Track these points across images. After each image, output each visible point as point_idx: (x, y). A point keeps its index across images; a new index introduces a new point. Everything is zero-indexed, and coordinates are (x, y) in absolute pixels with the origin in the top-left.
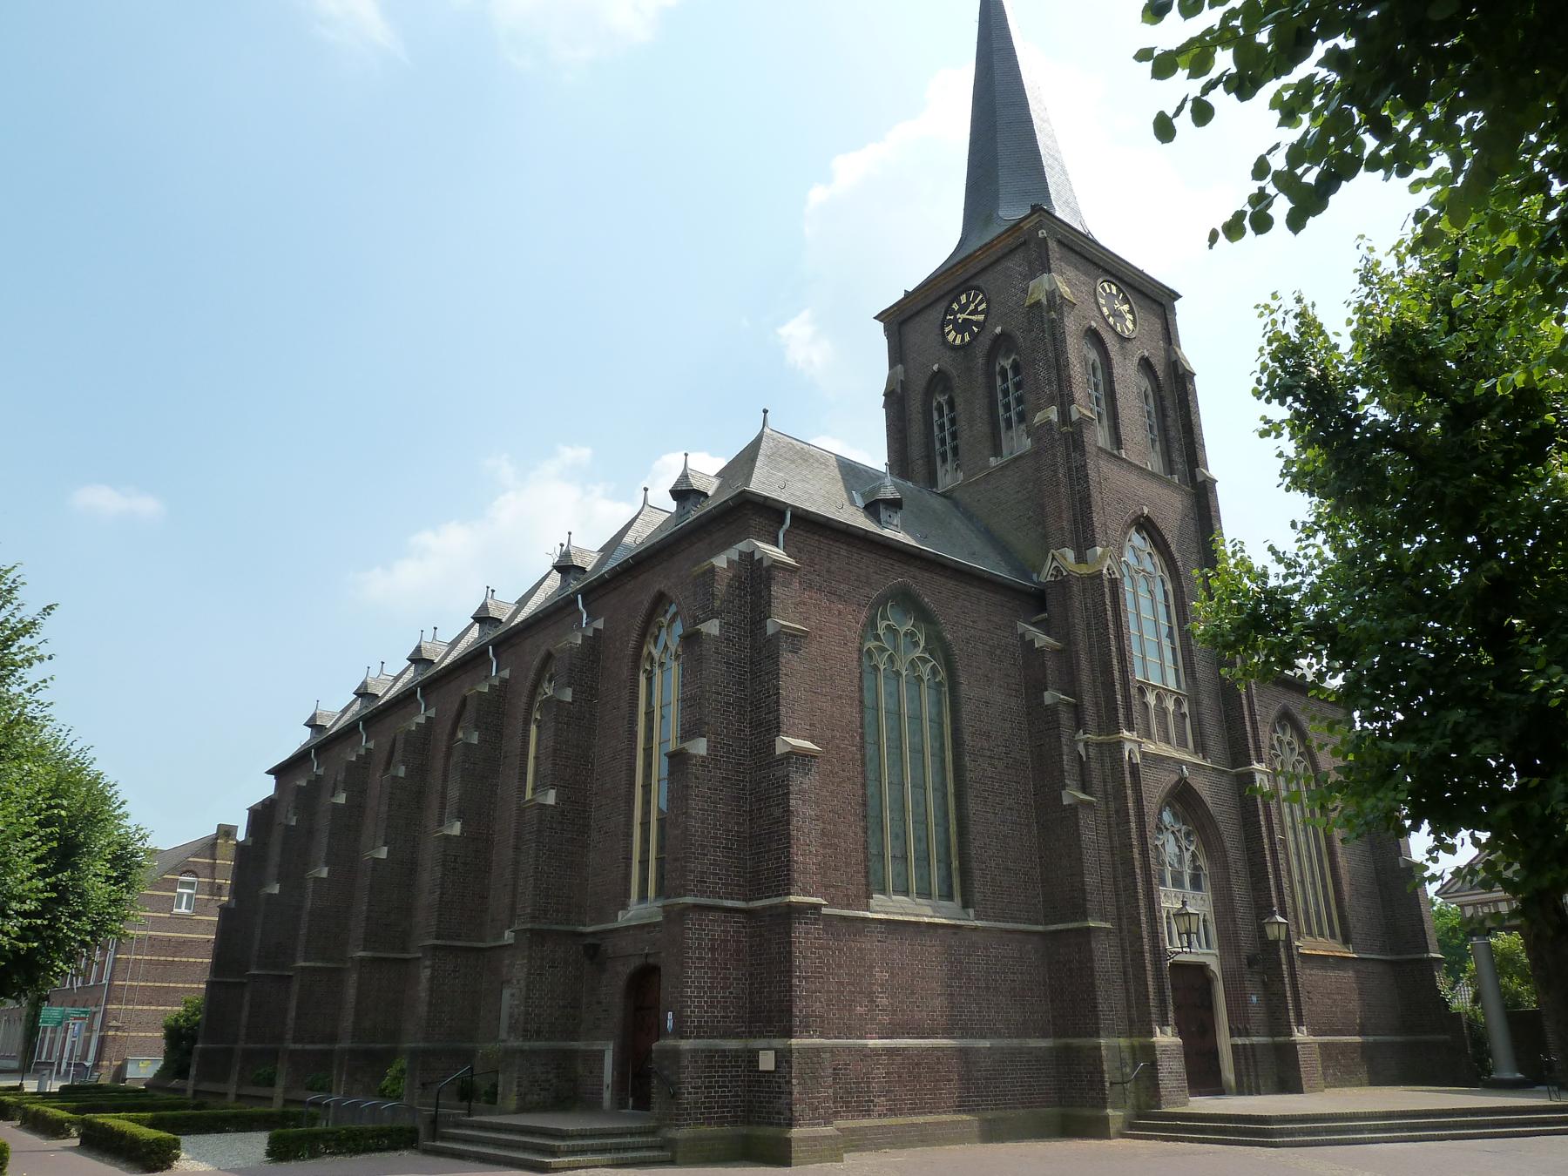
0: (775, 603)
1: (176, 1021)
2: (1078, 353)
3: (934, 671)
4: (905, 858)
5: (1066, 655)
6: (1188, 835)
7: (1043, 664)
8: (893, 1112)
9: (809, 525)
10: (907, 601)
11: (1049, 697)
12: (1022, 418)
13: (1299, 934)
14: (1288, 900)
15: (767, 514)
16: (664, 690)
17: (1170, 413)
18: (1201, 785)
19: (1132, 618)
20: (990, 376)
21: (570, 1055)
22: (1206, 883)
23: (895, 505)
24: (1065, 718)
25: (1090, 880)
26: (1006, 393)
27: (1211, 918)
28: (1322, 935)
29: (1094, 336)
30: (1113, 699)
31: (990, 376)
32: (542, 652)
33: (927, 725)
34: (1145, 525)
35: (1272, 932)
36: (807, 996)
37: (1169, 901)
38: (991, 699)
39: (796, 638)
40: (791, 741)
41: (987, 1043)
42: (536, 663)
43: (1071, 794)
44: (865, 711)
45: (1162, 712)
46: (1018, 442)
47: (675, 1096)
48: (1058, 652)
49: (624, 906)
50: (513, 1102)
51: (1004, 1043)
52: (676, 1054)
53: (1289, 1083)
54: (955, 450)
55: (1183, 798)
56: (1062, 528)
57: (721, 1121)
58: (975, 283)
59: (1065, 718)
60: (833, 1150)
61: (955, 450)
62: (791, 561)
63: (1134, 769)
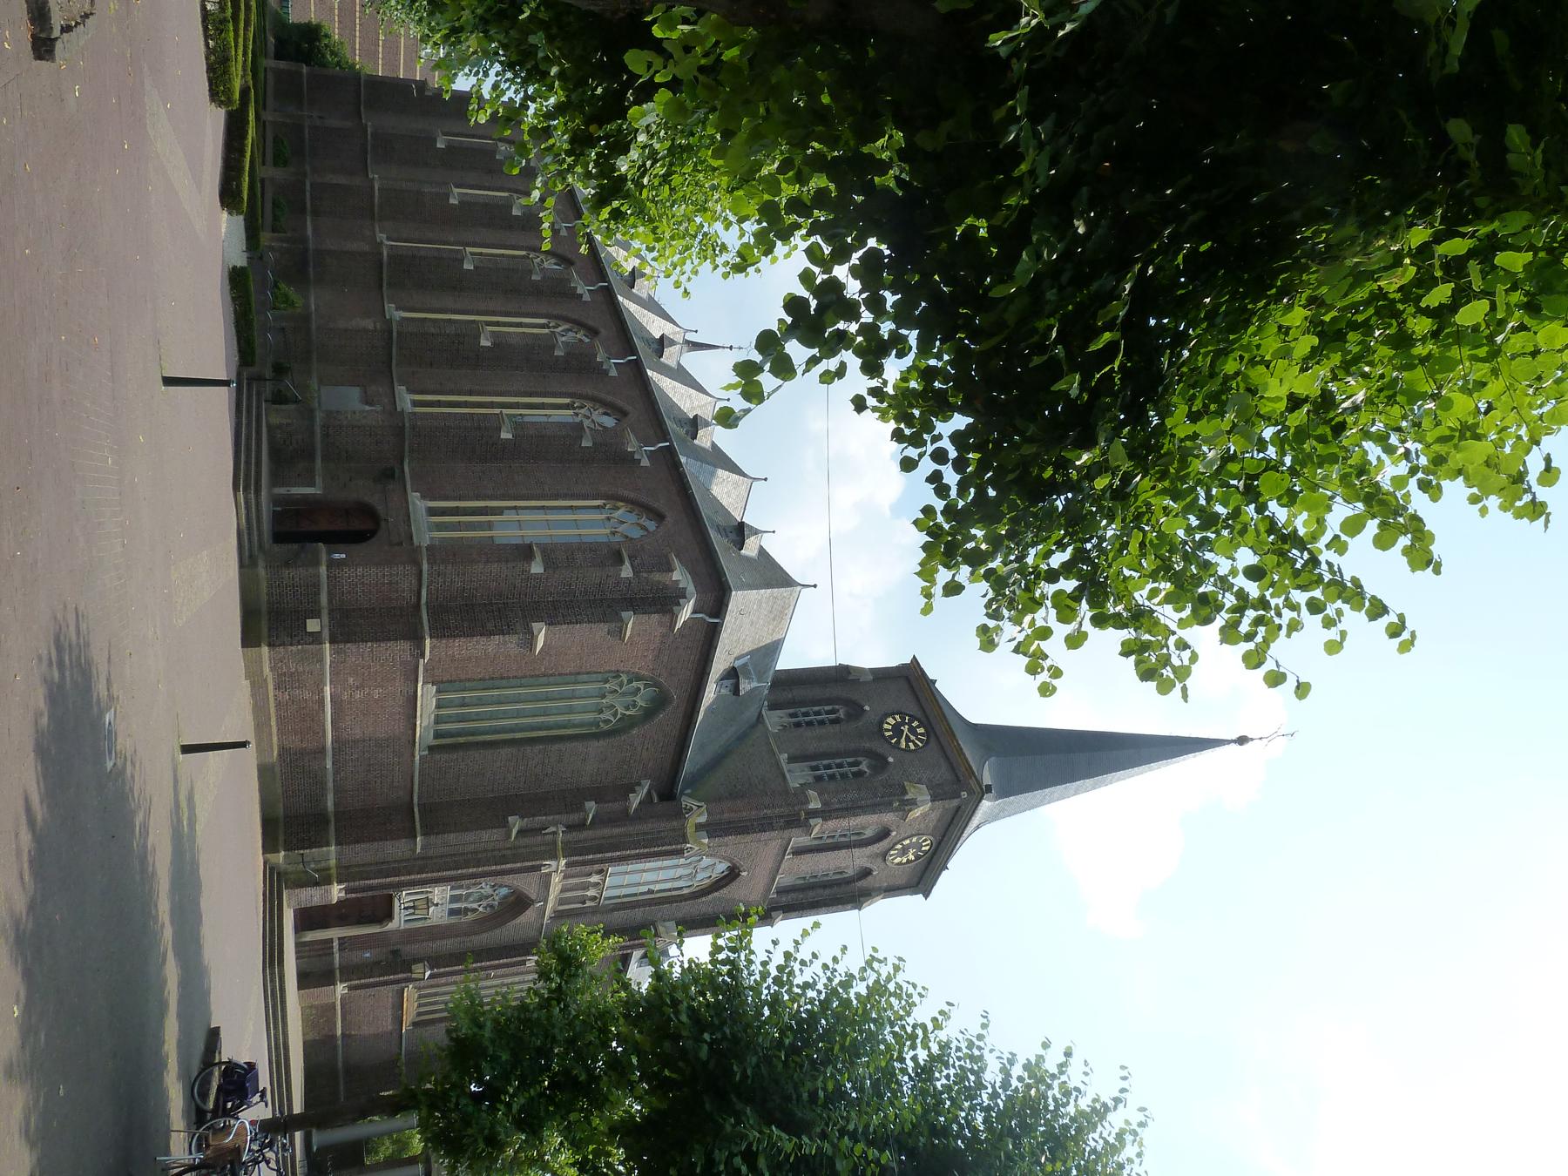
0: (646, 617)
1: (326, 36)
2: (869, 823)
3: (607, 721)
4: (463, 705)
5: (623, 817)
6: (492, 906)
7: (615, 800)
8: (278, 705)
9: (711, 636)
10: (660, 702)
11: (591, 806)
12: (819, 779)
13: (419, 989)
14: (443, 980)
15: (716, 601)
17: (827, 892)
18: (528, 916)
19: (659, 864)
20: (855, 753)
21: (311, 457)
22: (454, 919)
23: (736, 690)
24: (574, 818)
26: (840, 766)
27: (428, 923)
28: (420, 1006)
29: (884, 834)
30: (593, 850)
31: (855, 753)
32: (628, 408)
33: (566, 717)
34: (732, 874)
35: (418, 969)
36: (358, 653)
37: (440, 893)
38: (589, 762)
39: (620, 633)
41: (329, 765)
42: (619, 403)
43: (516, 823)
44: (574, 677)
45: (586, 887)
46: (797, 776)
47: (287, 564)
48: (626, 809)
49: (423, 497)
50: (275, 420)
51: (330, 778)
52: (317, 564)
53: (305, 980)
54: (798, 725)
55: (518, 903)
56: (723, 812)
57: (270, 594)
58: (933, 739)
59: (574, 818)
60: (254, 676)
61: (798, 725)
62: (679, 625)
63: (538, 868)
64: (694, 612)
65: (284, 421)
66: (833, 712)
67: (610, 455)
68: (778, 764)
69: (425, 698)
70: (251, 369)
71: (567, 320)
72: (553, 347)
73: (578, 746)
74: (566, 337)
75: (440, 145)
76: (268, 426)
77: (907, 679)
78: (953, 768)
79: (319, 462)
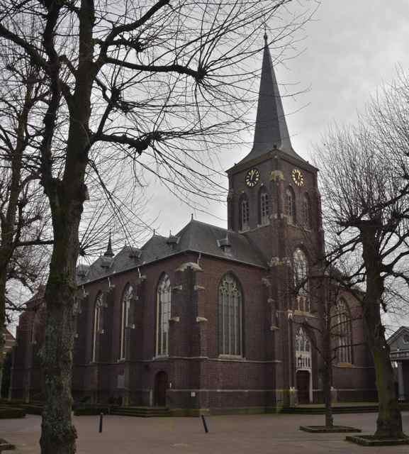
3: (238, 294)
10: (232, 275)
16: (165, 298)
25: (276, 350)
40: (199, 319)
42: (125, 284)
43: (273, 327)
46: (266, 222)
49: (155, 356)
58: (257, 167)
59: (273, 307)
61: (248, 219)
64: (197, 263)
66: (244, 205)
67: (142, 289)
68: (261, 228)
71: (96, 301)
72: (104, 308)
74: (101, 302)
75: (35, 342)
77: (233, 175)
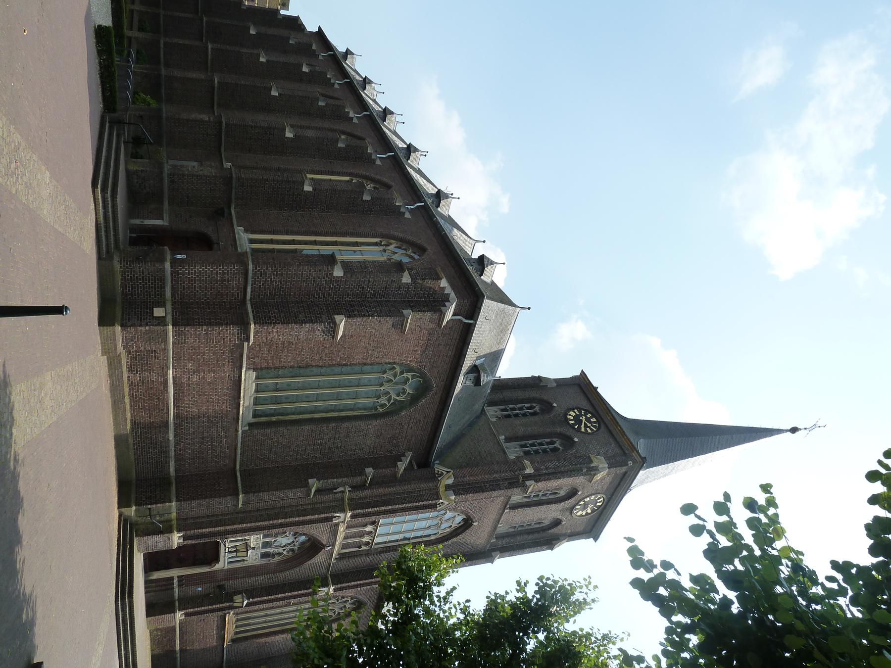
0: (421, 314)
2: (564, 484)
3: (383, 405)
4: (277, 390)
5: (393, 480)
6: (293, 550)
7: (388, 467)
8: (131, 384)
9: (465, 333)
10: (423, 390)
11: (369, 471)
12: (527, 453)
13: (237, 614)
14: (256, 607)
16: (371, 252)
17: (531, 537)
18: (321, 557)
22: (265, 561)
23: (477, 382)
24: (358, 480)
25: (266, 495)
26: (541, 444)
27: (245, 564)
28: (237, 627)
29: (573, 493)
30: (369, 507)
33: (352, 402)
34: (467, 524)
35: (238, 599)
36: (197, 335)
37: (255, 540)
38: (367, 438)
40: (342, 324)
41: (171, 438)
42: (385, 180)
44: (359, 366)
45: (362, 535)
46: (513, 452)
47: (138, 260)
48: (394, 475)
49: (246, 231)
50: (133, 167)
52: (162, 260)
53: (152, 609)
54: (508, 416)
55: (313, 547)
56: (465, 477)
57: (124, 286)
58: (603, 426)
59: (358, 480)
60: (108, 350)
61: (508, 416)
62: (444, 323)
63: (329, 519)
64: (454, 315)
65: (140, 169)
66: (531, 408)
68: (499, 443)
69: (245, 381)
70: (113, 115)
73: (361, 424)
76: (127, 171)
78: (620, 446)
79: (166, 203)
